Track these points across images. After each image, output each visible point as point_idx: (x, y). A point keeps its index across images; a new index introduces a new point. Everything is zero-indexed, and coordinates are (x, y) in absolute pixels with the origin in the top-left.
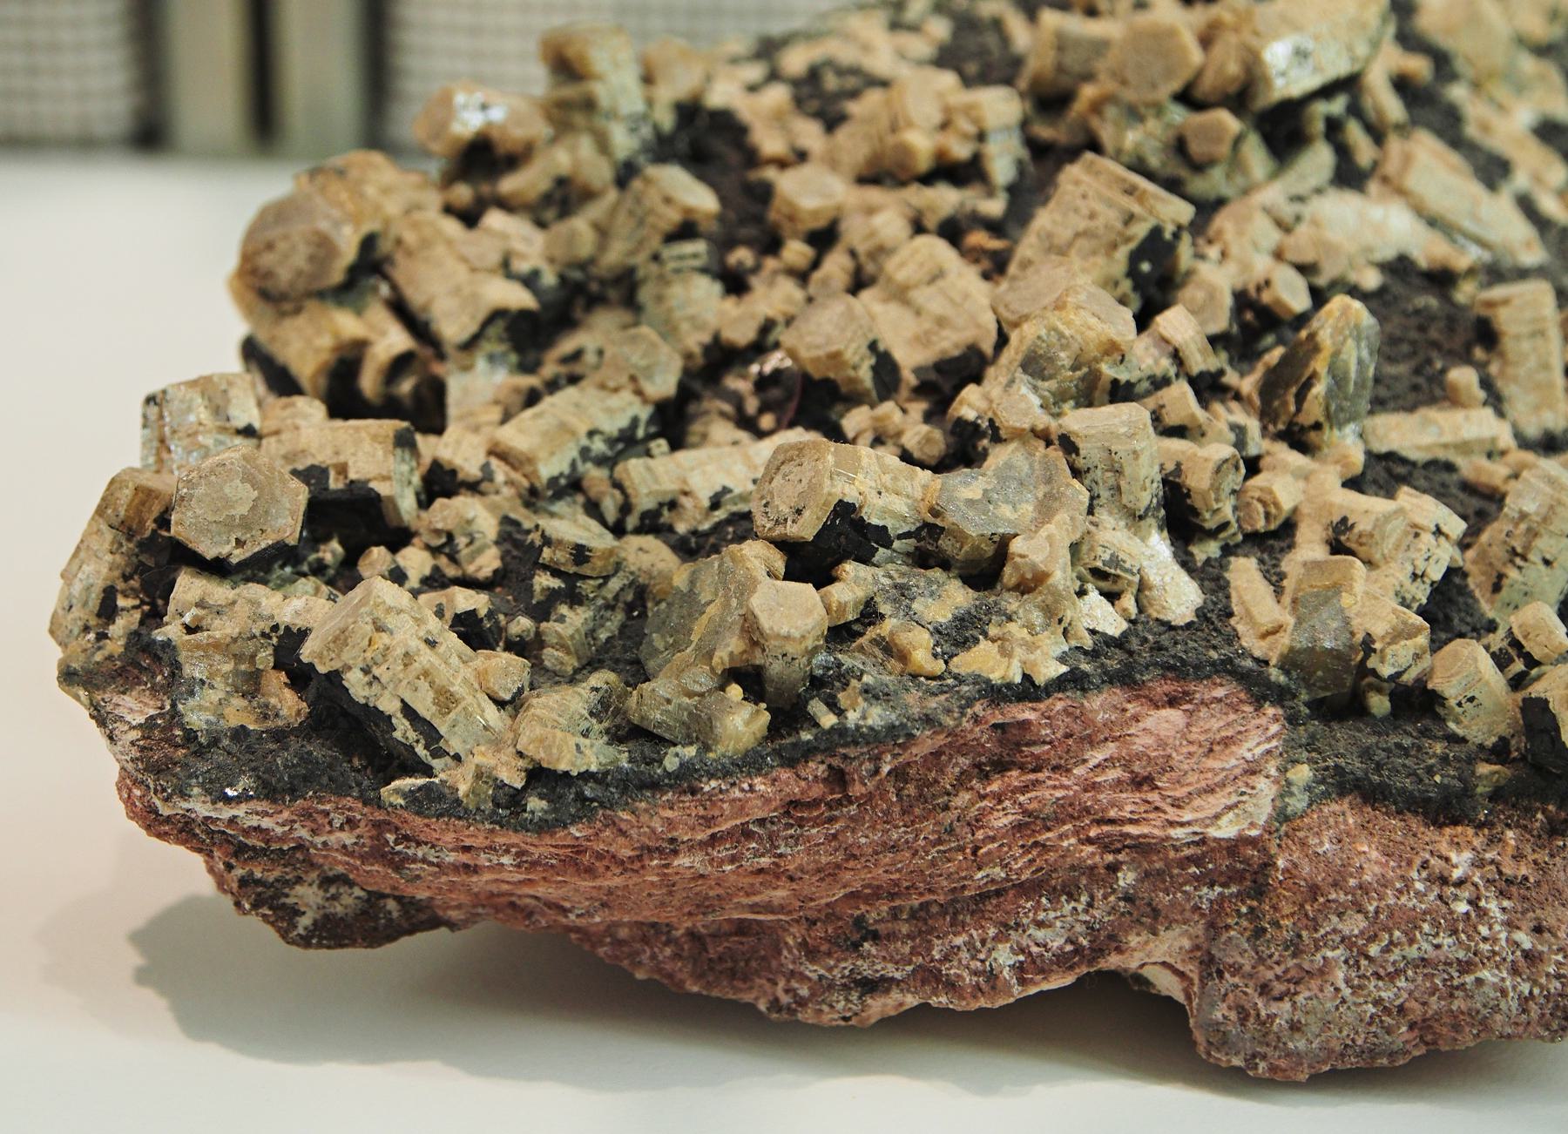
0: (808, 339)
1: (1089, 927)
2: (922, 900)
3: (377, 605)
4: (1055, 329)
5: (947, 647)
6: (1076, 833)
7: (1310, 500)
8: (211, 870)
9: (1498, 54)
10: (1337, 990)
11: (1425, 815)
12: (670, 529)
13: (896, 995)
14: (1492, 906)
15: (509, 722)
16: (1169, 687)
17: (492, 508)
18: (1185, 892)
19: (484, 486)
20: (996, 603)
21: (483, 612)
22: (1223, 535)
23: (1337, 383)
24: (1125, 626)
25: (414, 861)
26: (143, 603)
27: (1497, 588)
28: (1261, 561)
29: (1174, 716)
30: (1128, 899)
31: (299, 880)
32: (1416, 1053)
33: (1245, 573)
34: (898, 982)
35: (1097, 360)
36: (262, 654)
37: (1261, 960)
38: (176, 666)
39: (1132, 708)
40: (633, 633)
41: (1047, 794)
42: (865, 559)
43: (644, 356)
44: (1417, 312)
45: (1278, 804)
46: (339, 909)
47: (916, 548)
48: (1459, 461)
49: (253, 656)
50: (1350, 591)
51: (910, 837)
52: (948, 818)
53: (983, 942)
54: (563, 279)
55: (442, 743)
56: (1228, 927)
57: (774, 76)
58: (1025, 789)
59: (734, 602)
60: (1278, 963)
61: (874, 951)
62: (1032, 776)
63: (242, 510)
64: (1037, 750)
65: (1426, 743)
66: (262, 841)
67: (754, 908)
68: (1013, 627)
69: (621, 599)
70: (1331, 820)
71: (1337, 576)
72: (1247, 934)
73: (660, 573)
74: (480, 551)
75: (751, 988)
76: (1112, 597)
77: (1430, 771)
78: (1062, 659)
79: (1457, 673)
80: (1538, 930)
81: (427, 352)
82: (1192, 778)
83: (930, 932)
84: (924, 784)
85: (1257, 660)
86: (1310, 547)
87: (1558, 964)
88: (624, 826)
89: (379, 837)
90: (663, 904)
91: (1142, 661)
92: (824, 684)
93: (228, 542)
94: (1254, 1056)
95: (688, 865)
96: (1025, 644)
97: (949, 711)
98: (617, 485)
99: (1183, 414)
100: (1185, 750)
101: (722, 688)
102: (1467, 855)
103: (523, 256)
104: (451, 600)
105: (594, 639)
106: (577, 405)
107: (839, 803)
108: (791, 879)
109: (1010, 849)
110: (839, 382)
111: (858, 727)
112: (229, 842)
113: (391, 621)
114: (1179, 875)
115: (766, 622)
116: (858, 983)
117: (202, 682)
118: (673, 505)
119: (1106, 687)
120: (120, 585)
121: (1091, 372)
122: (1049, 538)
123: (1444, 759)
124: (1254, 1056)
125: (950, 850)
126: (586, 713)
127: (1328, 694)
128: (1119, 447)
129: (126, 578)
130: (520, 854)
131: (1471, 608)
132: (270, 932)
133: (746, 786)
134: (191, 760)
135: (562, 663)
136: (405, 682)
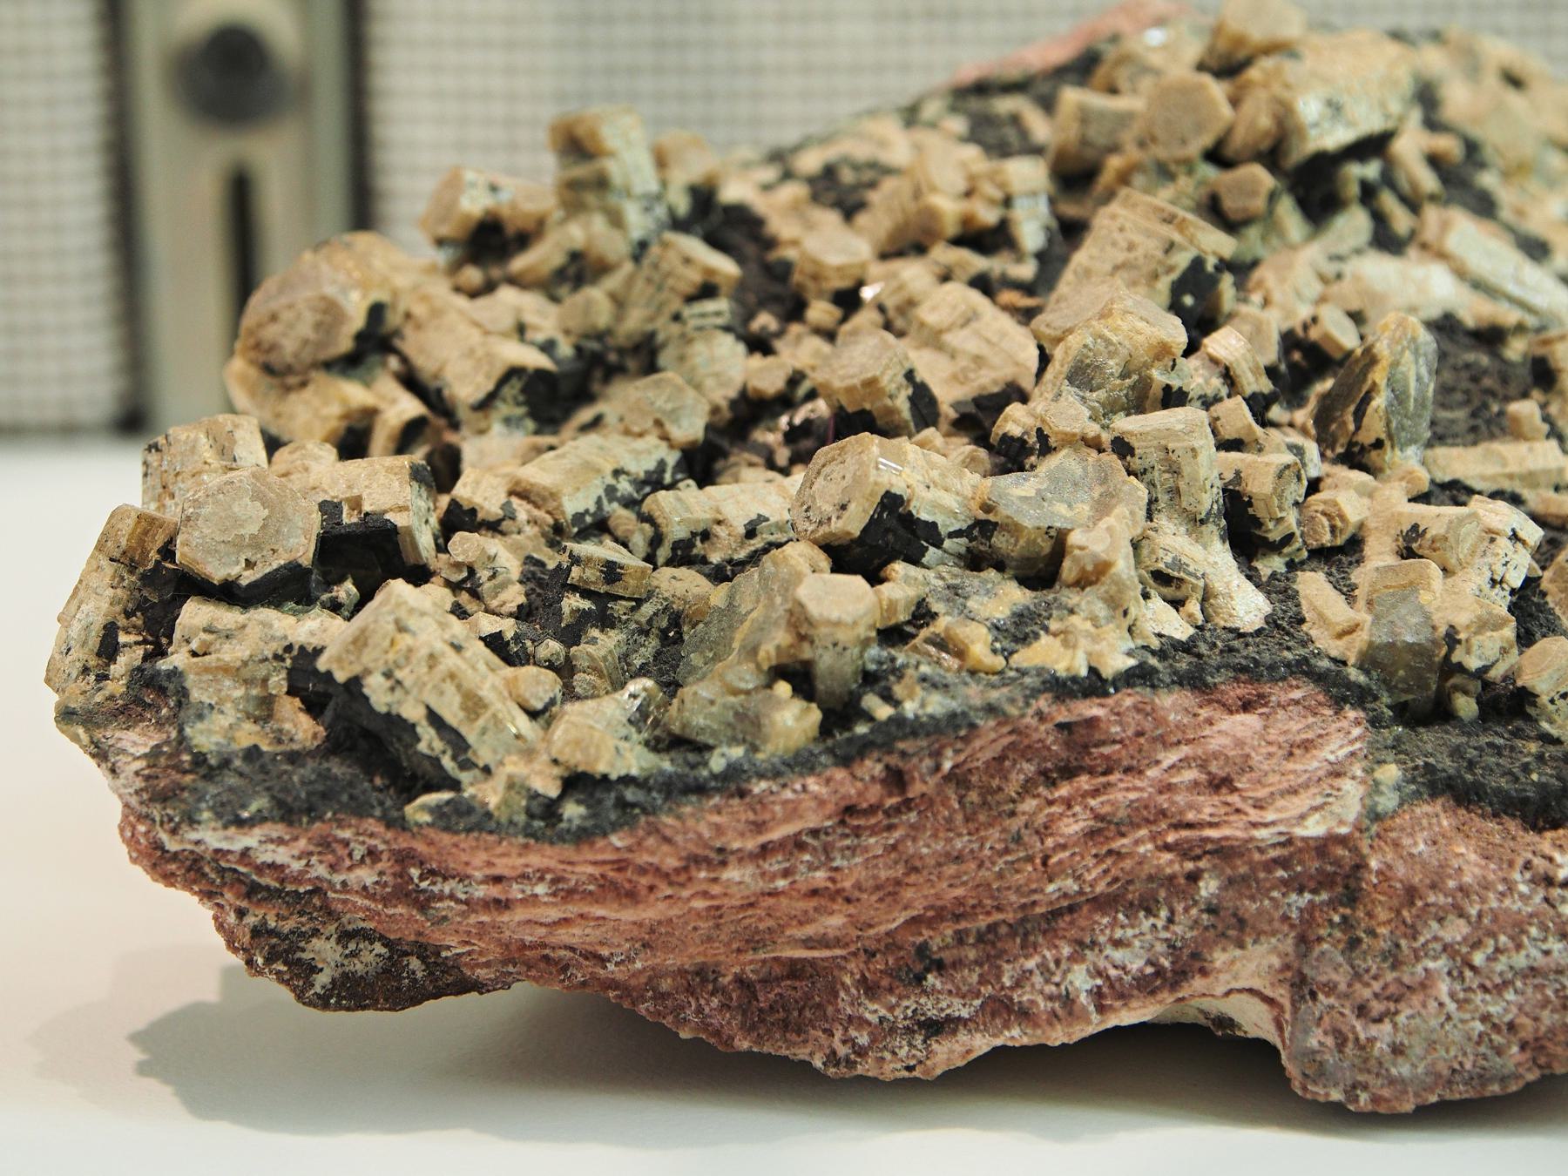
0: (841, 372)
2: (990, 920)
3: (398, 605)
5: (1007, 644)
6: (1153, 838)
7: (1375, 515)
8: (220, 927)
9: (1528, 149)
10: (1441, 1005)
11: (1524, 819)
12: (704, 560)
13: (963, 1036)
15: (541, 733)
16: (1243, 690)
17: (514, 548)
18: (1272, 899)
19: (505, 525)
20: (1055, 599)
21: (509, 635)
22: (1286, 550)
23: (1396, 397)
24: (1192, 631)
25: (441, 898)
26: (145, 642)
28: (1329, 574)
29: (1246, 723)
30: (1212, 910)
31: (316, 933)
33: (1314, 586)
35: (1147, 366)
36: (274, 679)
37: (1357, 976)
38: (183, 693)
39: (1204, 713)
41: (1120, 796)
42: (915, 560)
43: (668, 400)
44: (1467, 366)
45: (1368, 802)
46: (359, 967)
47: (968, 549)
49: (265, 681)
50: (1428, 588)
51: (975, 846)
52: (1015, 824)
53: (1058, 962)
54: (579, 349)
55: (470, 754)
56: (1320, 939)
57: (788, 175)
58: (1096, 793)
59: (778, 600)
60: (1375, 978)
61: (939, 985)
62: (1103, 779)
63: (253, 529)
64: (1106, 750)
65: (1519, 743)
66: (277, 879)
67: (808, 943)
68: (1074, 619)
69: (655, 624)
70: (1425, 822)
71: (1412, 576)
72: (1341, 946)
73: (695, 596)
74: (504, 586)
75: (805, 1041)
76: (1177, 604)
77: (1526, 769)
78: (1130, 654)
79: (1548, 667)
81: (441, 422)
82: (1273, 778)
83: (999, 956)
84: (986, 791)
85: (1334, 660)
86: (1379, 554)
88: (668, 832)
89: (402, 874)
90: (709, 939)
91: (1212, 662)
93: (237, 563)
94: (1354, 1087)
95: (738, 879)
96: (1088, 635)
97: (1012, 701)
98: (648, 519)
99: (1239, 424)
100: (1264, 751)
101: (769, 686)
103: (536, 328)
105: (628, 664)
106: (601, 448)
107: (897, 810)
108: (848, 900)
109: (1083, 858)
110: (875, 414)
111: (917, 717)
112: (243, 883)
113: (412, 623)
114: (1266, 879)
115: (814, 609)
116: (921, 1025)
117: (211, 707)
118: (706, 535)
119: (1177, 688)
120: (122, 622)
122: (1109, 529)
123: (1540, 758)
124: (1354, 1087)
125: (1018, 860)
127: (1410, 697)
129: (128, 614)
130: (555, 881)
132: (286, 994)
133: (798, 787)
134: (201, 784)
135: (594, 687)
136: (429, 686)
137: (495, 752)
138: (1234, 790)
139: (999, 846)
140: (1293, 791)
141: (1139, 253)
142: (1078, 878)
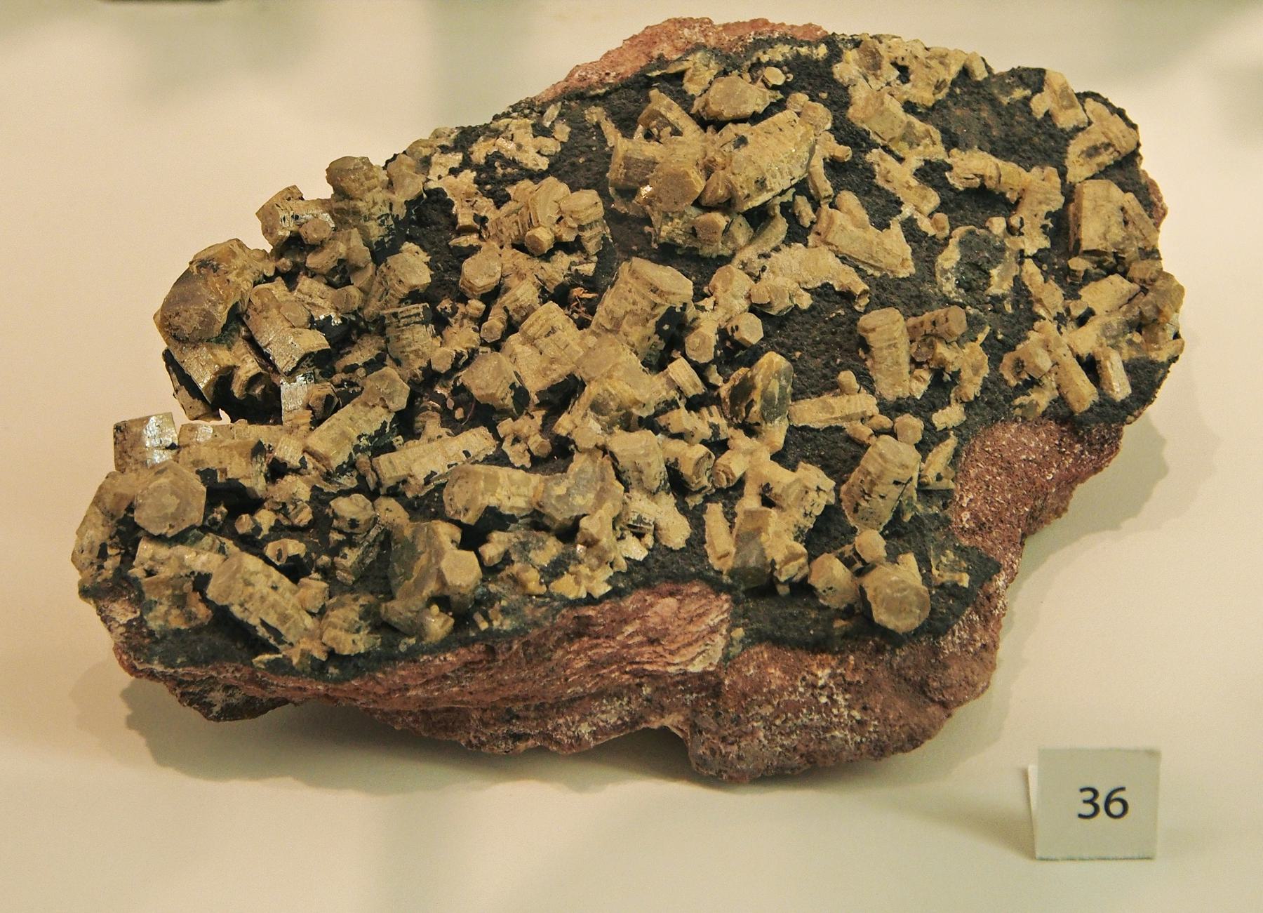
1: (630, 713)
4: (607, 390)
11: (807, 649)
14: (840, 699)
15: (318, 623)
17: (307, 482)
19: (302, 471)
21: (303, 555)
24: (646, 553)
25: (272, 684)
27: (856, 511)
28: (725, 505)
29: (671, 602)
30: (648, 700)
31: (212, 690)
32: (805, 768)
34: (532, 736)
40: (383, 560)
48: (845, 425)
52: (550, 665)
53: (573, 723)
56: (702, 712)
57: (466, 163)
58: (591, 648)
62: (595, 642)
63: (171, 510)
64: (597, 629)
70: (755, 657)
71: (760, 522)
74: (301, 510)
76: (640, 536)
78: (609, 582)
80: (865, 708)
84: (538, 646)
86: (750, 501)
87: (875, 726)
92: (484, 602)
94: (720, 771)
102: (828, 671)
104: (286, 548)
113: (253, 579)
117: (156, 602)
118: (405, 482)
121: (627, 412)
123: (816, 621)
126: (357, 619)
128: (640, 462)
131: (843, 522)
137: (295, 636)
138: (660, 644)
139: (543, 674)
140: (690, 644)
141: (639, 307)
142: (583, 686)
